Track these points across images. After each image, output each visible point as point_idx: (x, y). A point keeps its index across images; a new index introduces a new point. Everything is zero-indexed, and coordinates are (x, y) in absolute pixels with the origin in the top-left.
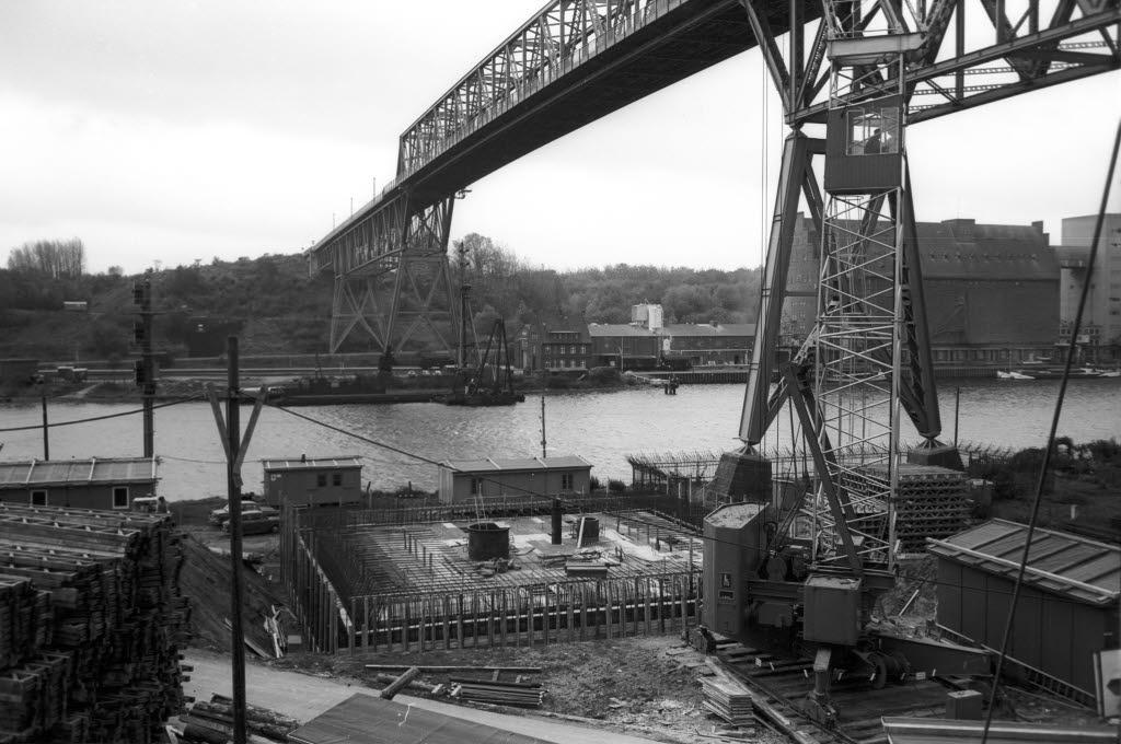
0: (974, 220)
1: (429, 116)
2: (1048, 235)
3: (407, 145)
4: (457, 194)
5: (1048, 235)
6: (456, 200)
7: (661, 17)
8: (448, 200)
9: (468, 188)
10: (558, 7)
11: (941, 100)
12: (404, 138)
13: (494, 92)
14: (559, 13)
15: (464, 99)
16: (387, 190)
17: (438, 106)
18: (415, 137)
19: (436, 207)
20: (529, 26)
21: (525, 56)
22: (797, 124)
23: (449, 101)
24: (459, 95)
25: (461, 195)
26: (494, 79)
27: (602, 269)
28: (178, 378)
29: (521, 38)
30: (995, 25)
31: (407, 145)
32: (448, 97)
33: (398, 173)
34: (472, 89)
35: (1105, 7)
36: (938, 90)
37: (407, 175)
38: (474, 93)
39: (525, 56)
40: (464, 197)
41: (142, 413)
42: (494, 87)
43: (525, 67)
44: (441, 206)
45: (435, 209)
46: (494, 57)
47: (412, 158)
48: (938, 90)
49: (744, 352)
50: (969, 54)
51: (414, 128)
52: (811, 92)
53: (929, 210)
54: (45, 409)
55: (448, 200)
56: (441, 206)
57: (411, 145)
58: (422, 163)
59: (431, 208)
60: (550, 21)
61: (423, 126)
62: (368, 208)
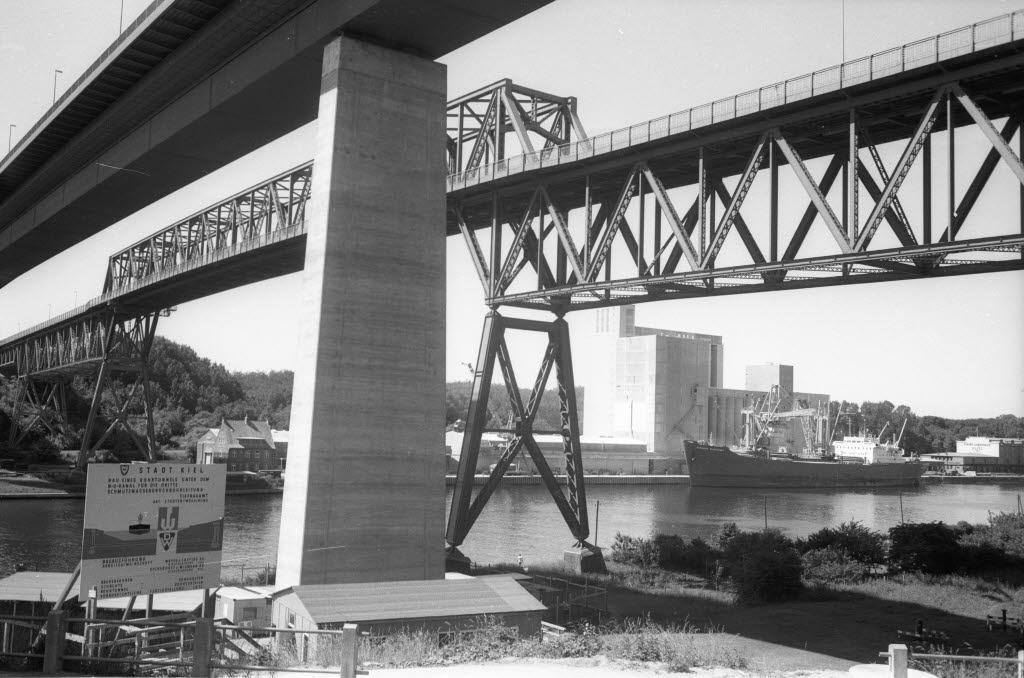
0: (827, 397)
3: (118, 266)
4: (162, 312)
7: (470, 187)
8: (152, 319)
9: (173, 308)
11: (596, 299)
12: (114, 259)
14: (289, 183)
15: (185, 234)
18: (127, 259)
19: (139, 321)
21: (190, 234)
22: (495, 306)
23: (167, 234)
24: (180, 231)
26: (219, 222)
27: (267, 372)
28: (37, 479)
29: (250, 195)
30: (536, 270)
31: (118, 266)
32: (168, 231)
34: (195, 228)
35: (706, 268)
36: (597, 295)
37: (115, 294)
38: (197, 232)
40: (169, 315)
43: (189, 240)
44: (144, 322)
48: (597, 295)
49: (90, 356)
50: (718, 270)
52: (506, 284)
53: (159, 333)
55: (152, 319)
56: (144, 322)
57: (121, 267)
59: (133, 321)
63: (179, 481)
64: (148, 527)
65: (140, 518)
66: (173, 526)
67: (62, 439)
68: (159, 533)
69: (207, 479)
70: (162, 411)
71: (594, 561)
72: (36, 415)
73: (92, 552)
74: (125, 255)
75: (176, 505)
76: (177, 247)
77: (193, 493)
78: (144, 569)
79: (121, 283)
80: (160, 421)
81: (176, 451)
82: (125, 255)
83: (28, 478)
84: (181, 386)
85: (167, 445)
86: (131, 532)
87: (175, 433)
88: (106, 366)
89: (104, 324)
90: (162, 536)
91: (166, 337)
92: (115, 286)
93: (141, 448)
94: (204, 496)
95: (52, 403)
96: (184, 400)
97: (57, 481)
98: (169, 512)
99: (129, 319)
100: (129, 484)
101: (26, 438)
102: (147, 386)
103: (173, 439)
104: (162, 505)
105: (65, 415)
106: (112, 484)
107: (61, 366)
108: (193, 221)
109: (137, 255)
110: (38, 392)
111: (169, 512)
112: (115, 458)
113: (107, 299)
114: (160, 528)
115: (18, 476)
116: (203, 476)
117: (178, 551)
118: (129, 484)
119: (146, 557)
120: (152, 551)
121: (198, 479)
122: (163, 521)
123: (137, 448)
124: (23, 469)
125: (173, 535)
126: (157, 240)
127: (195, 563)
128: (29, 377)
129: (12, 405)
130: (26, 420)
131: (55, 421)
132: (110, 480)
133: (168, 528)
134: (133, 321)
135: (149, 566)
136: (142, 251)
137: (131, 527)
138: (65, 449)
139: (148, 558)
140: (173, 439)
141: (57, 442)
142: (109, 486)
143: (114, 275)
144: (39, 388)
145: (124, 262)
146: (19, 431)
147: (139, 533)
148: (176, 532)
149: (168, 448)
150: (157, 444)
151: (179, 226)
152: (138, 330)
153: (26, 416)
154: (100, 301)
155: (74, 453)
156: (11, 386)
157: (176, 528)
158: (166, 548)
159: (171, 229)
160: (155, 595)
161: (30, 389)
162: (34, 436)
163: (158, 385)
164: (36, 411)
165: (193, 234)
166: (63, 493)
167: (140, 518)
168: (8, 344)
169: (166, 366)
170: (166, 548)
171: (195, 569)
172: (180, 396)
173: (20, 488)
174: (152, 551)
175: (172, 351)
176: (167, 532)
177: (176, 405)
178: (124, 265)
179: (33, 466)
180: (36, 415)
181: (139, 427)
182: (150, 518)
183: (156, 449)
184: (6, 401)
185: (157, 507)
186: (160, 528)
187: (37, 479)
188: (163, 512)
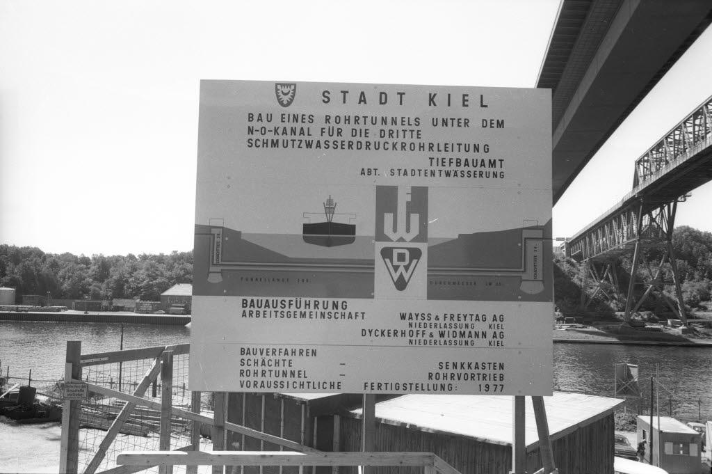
1: (659, 145)
2: (552, 395)
3: (641, 167)
4: (679, 199)
5: (552, 395)
6: (678, 203)
8: (672, 204)
9: (688, 194)
10: (692, 118)
12: (638, 162)
13: (675, 150)
15: (690, 129)
16: (626, 199)
17: (667, 137)
18: (647, 161)
19: (662, 208)
20: (669, 135)
21: (694, 129)
23: (677, 132)
24: (686, 127)
25: (683, 199)
28: (597, 330)
31: (641, 167)
32: (676, 129)
33: (634, 187)
34: (697, 122)
37: (641, 187)
38: (700, 125)
39: (694, 129)
40: (685, 200)
41: (661, 418)
42: (675, 147)
43: (694, 134)
44: (666, 208)
45: (661, 211)
46: (674, 131)
47: (645, 176)
51: (647, 155)
54: (121, 363)
55: (672, 204)
56: (666, 208)
57: (644, 167)
58: (654, 179)
59: (658, 210)
60: (688, 125)
61: (654, 152)
62: (617, 208)
63: (426, 126)
64: (350, 229)
65: (330, 207)
66: (415, 231)
67: (616, 304)
68: (380, 245)
69: (501, 124)
70: (691, 282)
71: (29, 386)
72: (598, 286)
73: (215, 278)
74: (646, 158)
75: (419, 181)
76: (685, 143)
77: (463, 156)
78: (345, 329)
79: (645, 178)
80: (690, 290)
81: (705, 313)
82: (646, 158)
83: (591, 329)
84: (706, 263)
85: (696, 308)
86: (306, 240)
87: (703, 300)
88: (639, 244)
89: (635, 213)
90: (386, 253)
91: (690, 226)
92: (641, 180)
93: (673, 309)
94: (492, 164)
95: (607, 279)
96: (709, 273)
97: (611, 332)
98: (403, 198)
99: (655, 208)
100: (298, 125)
101: (592, 303)
102: (673, 264)
103: (702, 304)
104: (386, 180)
105: (617, 286)
106: (256, 125)
107: (610, 249)
108: (696, 114)
109: (655, 156)
110: (597, 271)
111: (403, 198)
112: (657, 318)
113: (637, 191)
114: (380, 236)
115: (583, 327)
116: (487, 114)
117: (432, 295)
118: (298, 125)
119: (350, 301)
120: (365, 289)
121: (476, 123)
122: (388, 218)
123: (672, 311)
124: (589, 323)
125: (415, 254)
126: (670, 140)
127: (480, 327)
128: (591, 259)
129: (581, 280)
130: (592, 291)
131: (611, 292)
132: (251, 117)
133: (401, 233)
134: (658, 210)
135: (359, 324)
136: (658, 150)
137: (308, 229)
138: (619, 311)
139: (354, 305)
140: (702, 304)
141: (612, 305)
142: (251, 130)
143: (639, 175)
144: (598, 267)
145: (646, 164)
146: (587, 297)
147: (329, 243)
148: (423, 247)
149: (698, 311)
150: (688, 306)
151: (685, 123)
152: (662, 216)
153: (592, 288)
154: (631, 196)
155: (623, 313)
156: (580, 268)
157: (422, 237)
158: (401, 284)
159: (679, 127)
160: (547, 400)
161: (591, 268)
162: (596, 302)
163: (686, 263)
164: (598, 284)
165: (697, 128)
166: (614, 340)
167: (330, 207)
168: (577, 238)
169: (692, 248)
170: (401, 284)
171: (479, 342)
172: (705, 271)
173: (584, 335)
174: (365, 289)
175: (696, 236)
176: (398, 247)
177: (702, 277)
178: (645, 166)
179: (595, 322)
180: (598, 286)
181: (670, 293)
182: (357, 210)
183: (685, 310)
184: (578, 278)
185: (371, 183)
186: (380, 236)
187: (597, 330)
188: (386, 198)
